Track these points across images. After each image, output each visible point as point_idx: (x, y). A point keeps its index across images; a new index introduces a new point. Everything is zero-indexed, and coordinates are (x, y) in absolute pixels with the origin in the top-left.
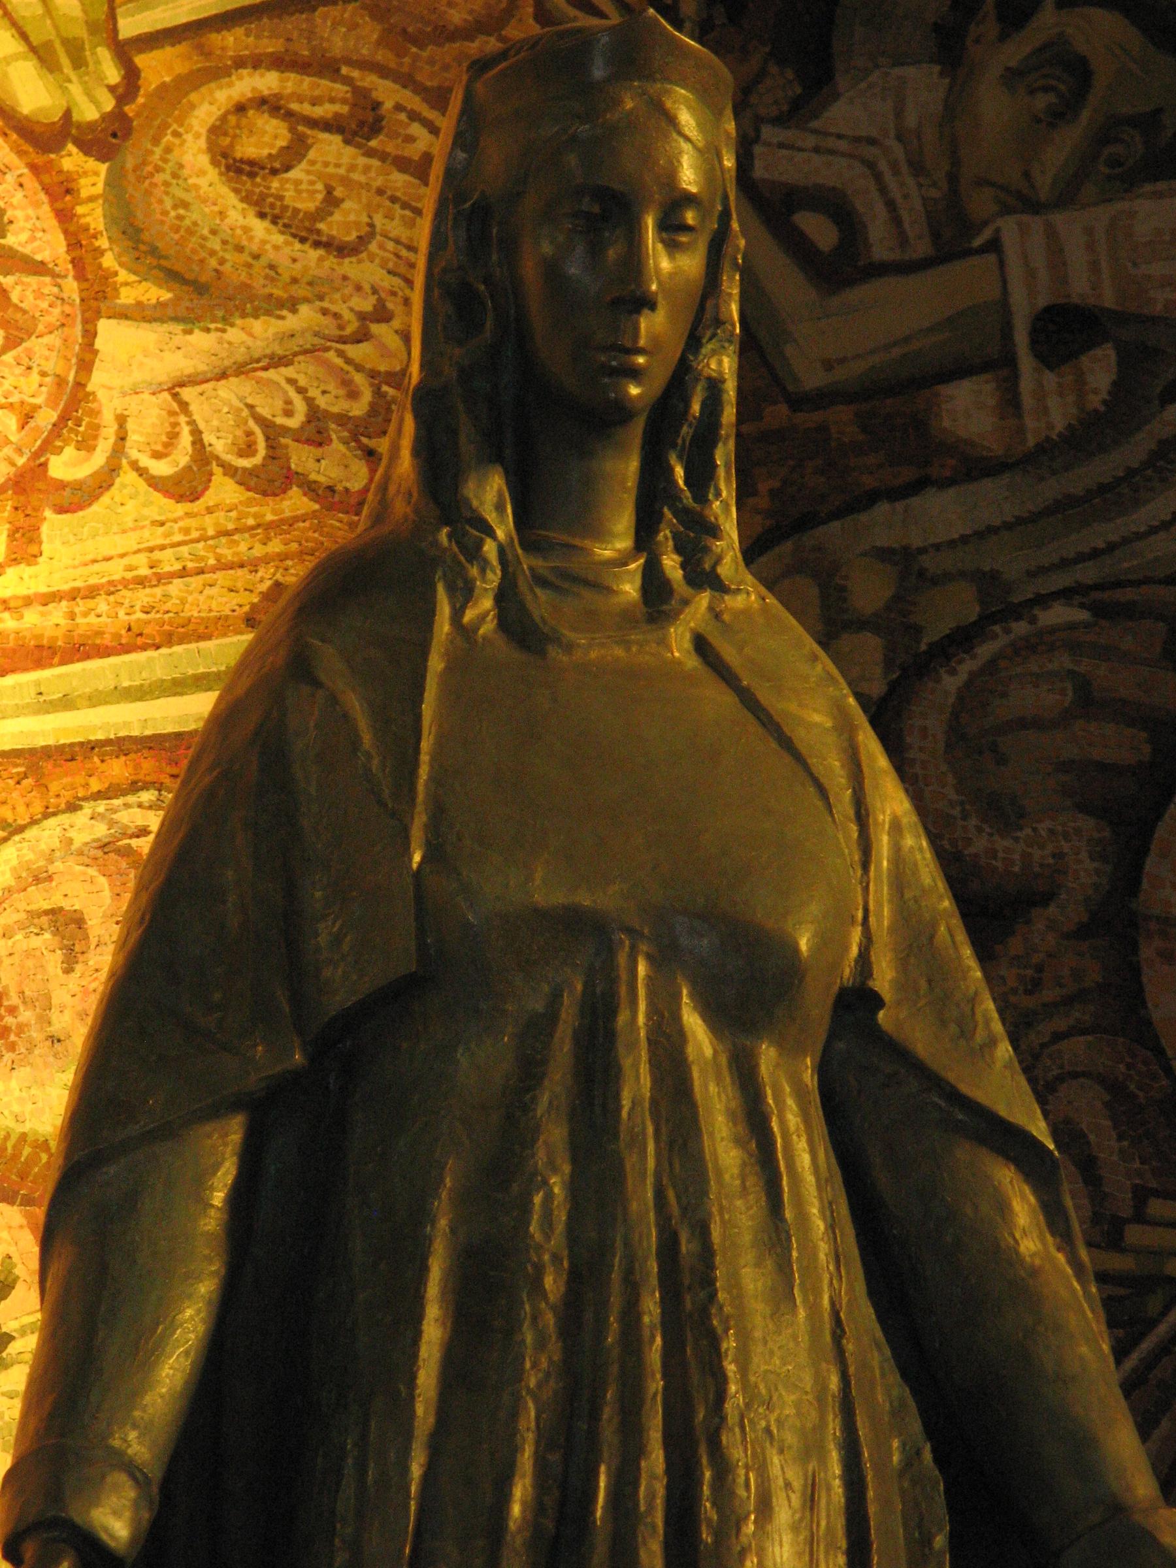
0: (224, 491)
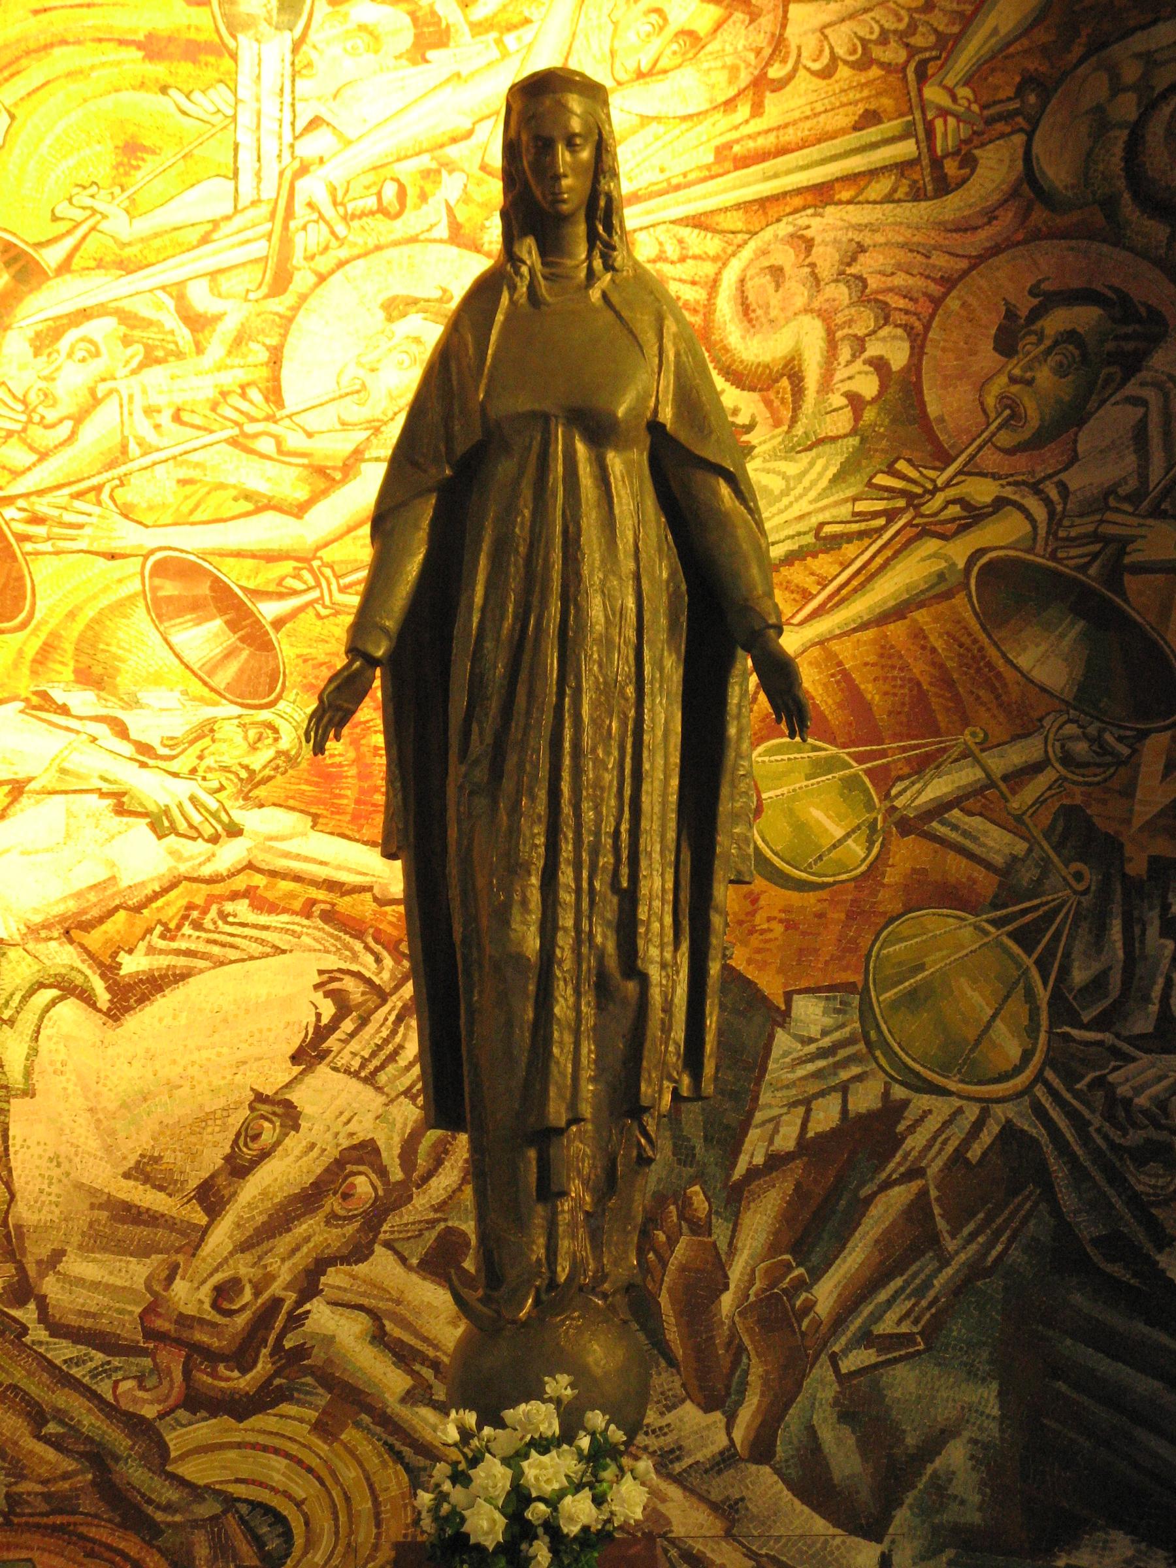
0: (844, 72)
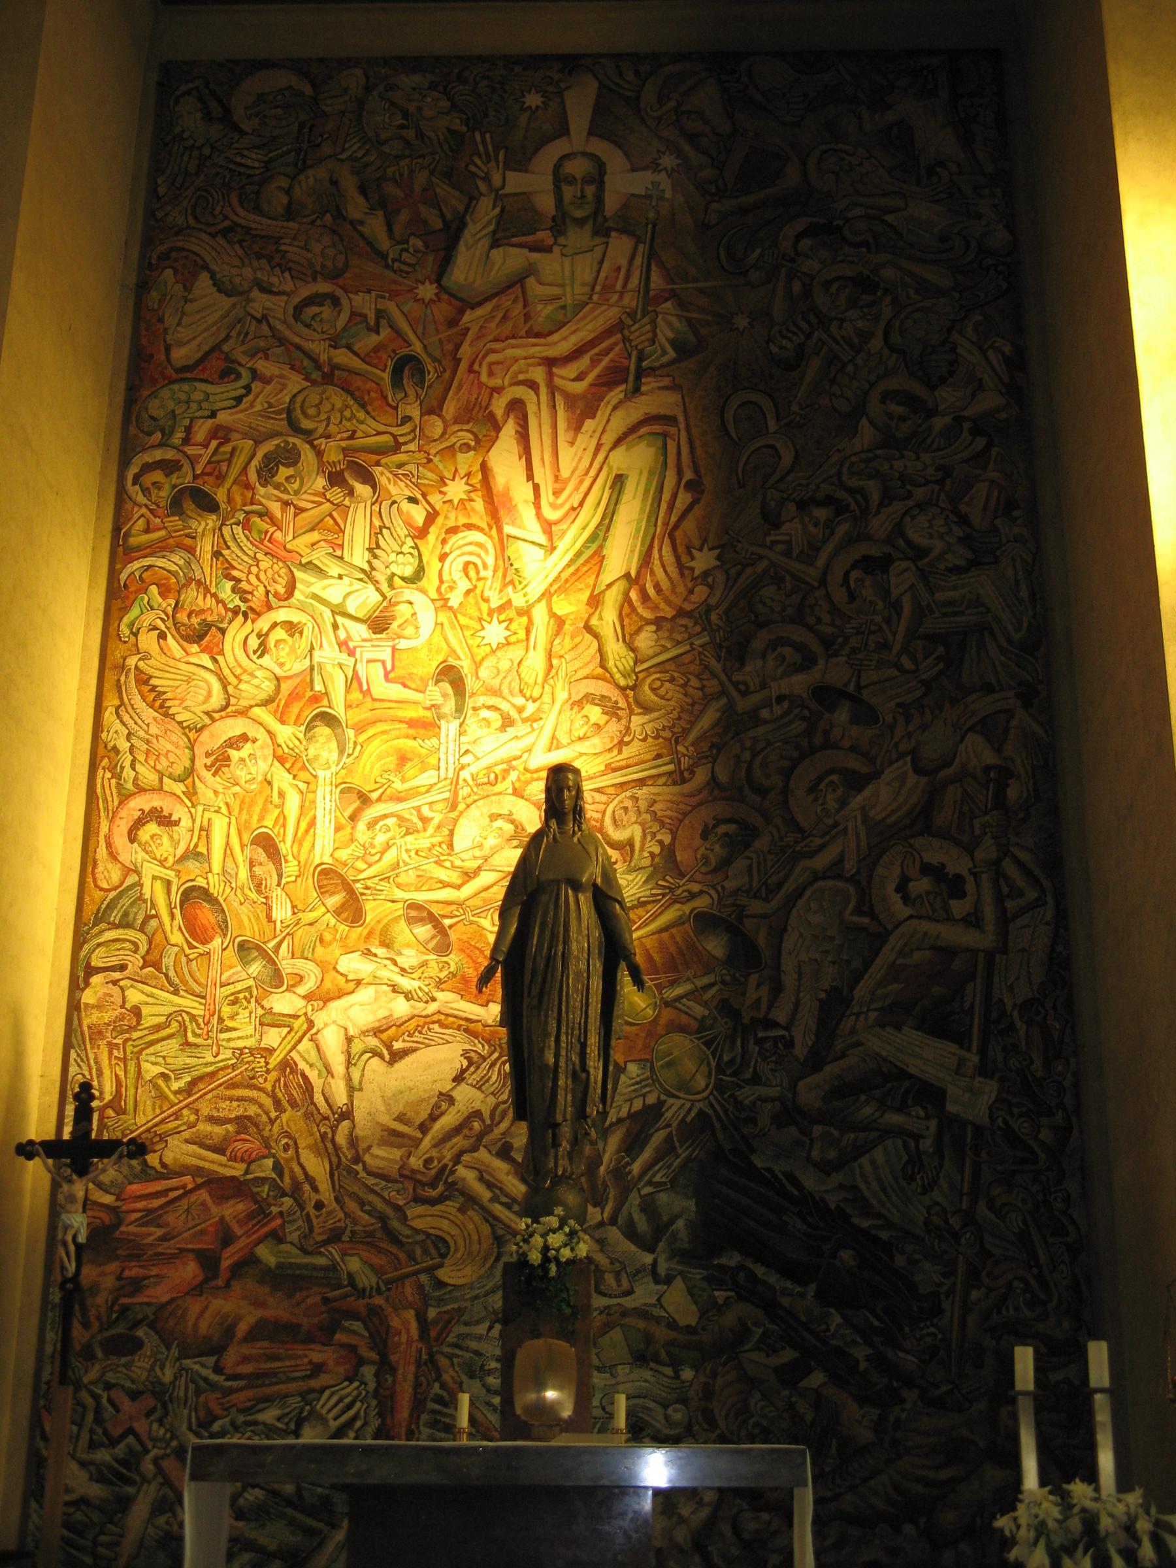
0: (650, 740)
